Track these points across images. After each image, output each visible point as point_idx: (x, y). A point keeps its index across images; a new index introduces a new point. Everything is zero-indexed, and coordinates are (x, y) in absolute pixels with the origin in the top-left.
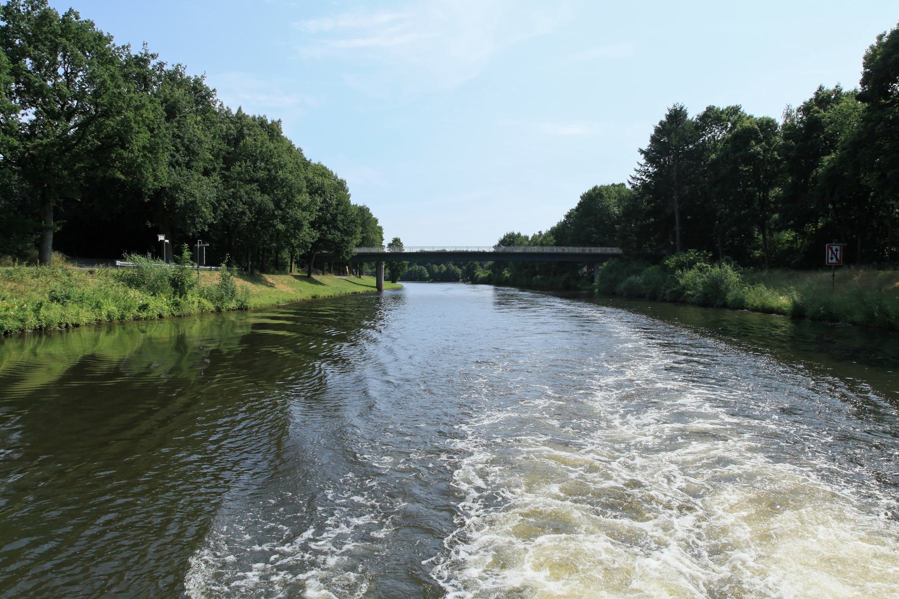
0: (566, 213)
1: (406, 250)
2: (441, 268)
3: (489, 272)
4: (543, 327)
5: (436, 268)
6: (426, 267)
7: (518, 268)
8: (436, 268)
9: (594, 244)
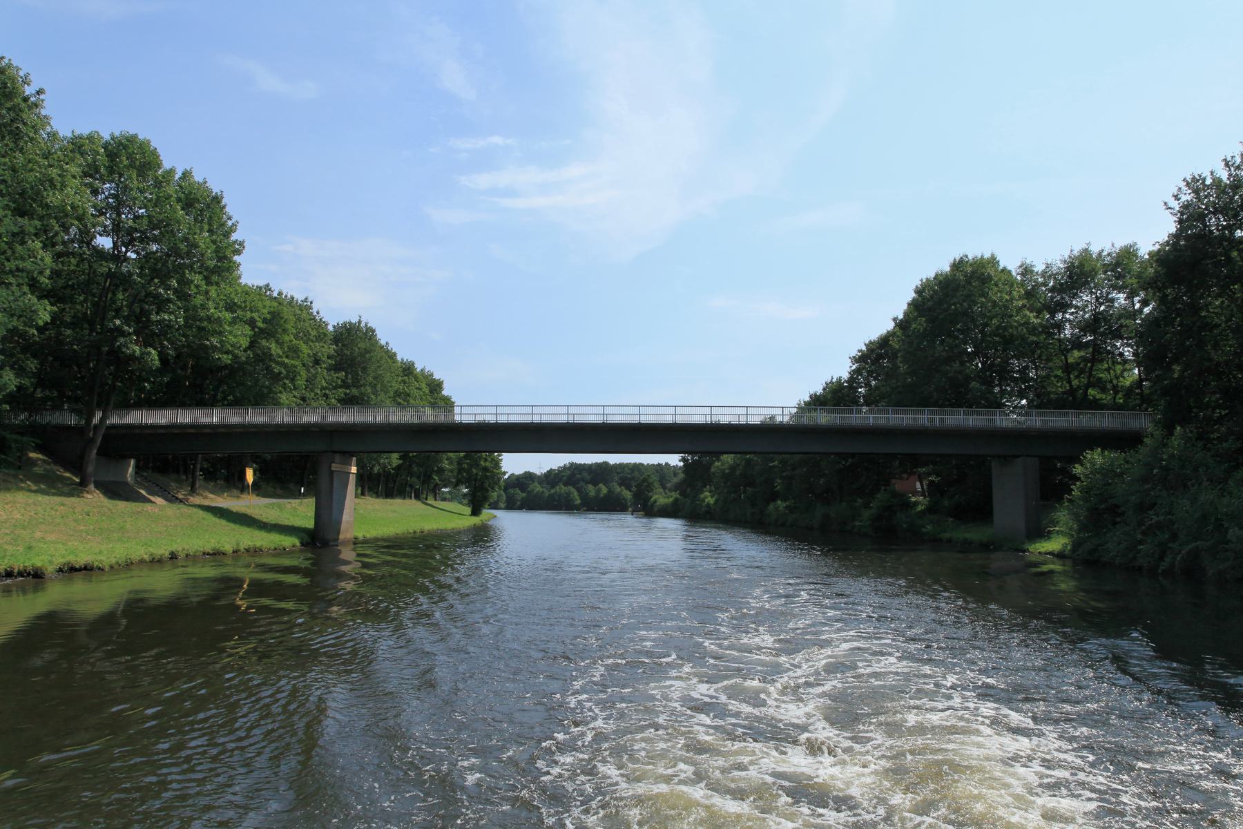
0: (854, 353)
1: (464, 415)
2: (599, 490)
3: (675, 495)
6: (579, 490)
8: (591, 491)
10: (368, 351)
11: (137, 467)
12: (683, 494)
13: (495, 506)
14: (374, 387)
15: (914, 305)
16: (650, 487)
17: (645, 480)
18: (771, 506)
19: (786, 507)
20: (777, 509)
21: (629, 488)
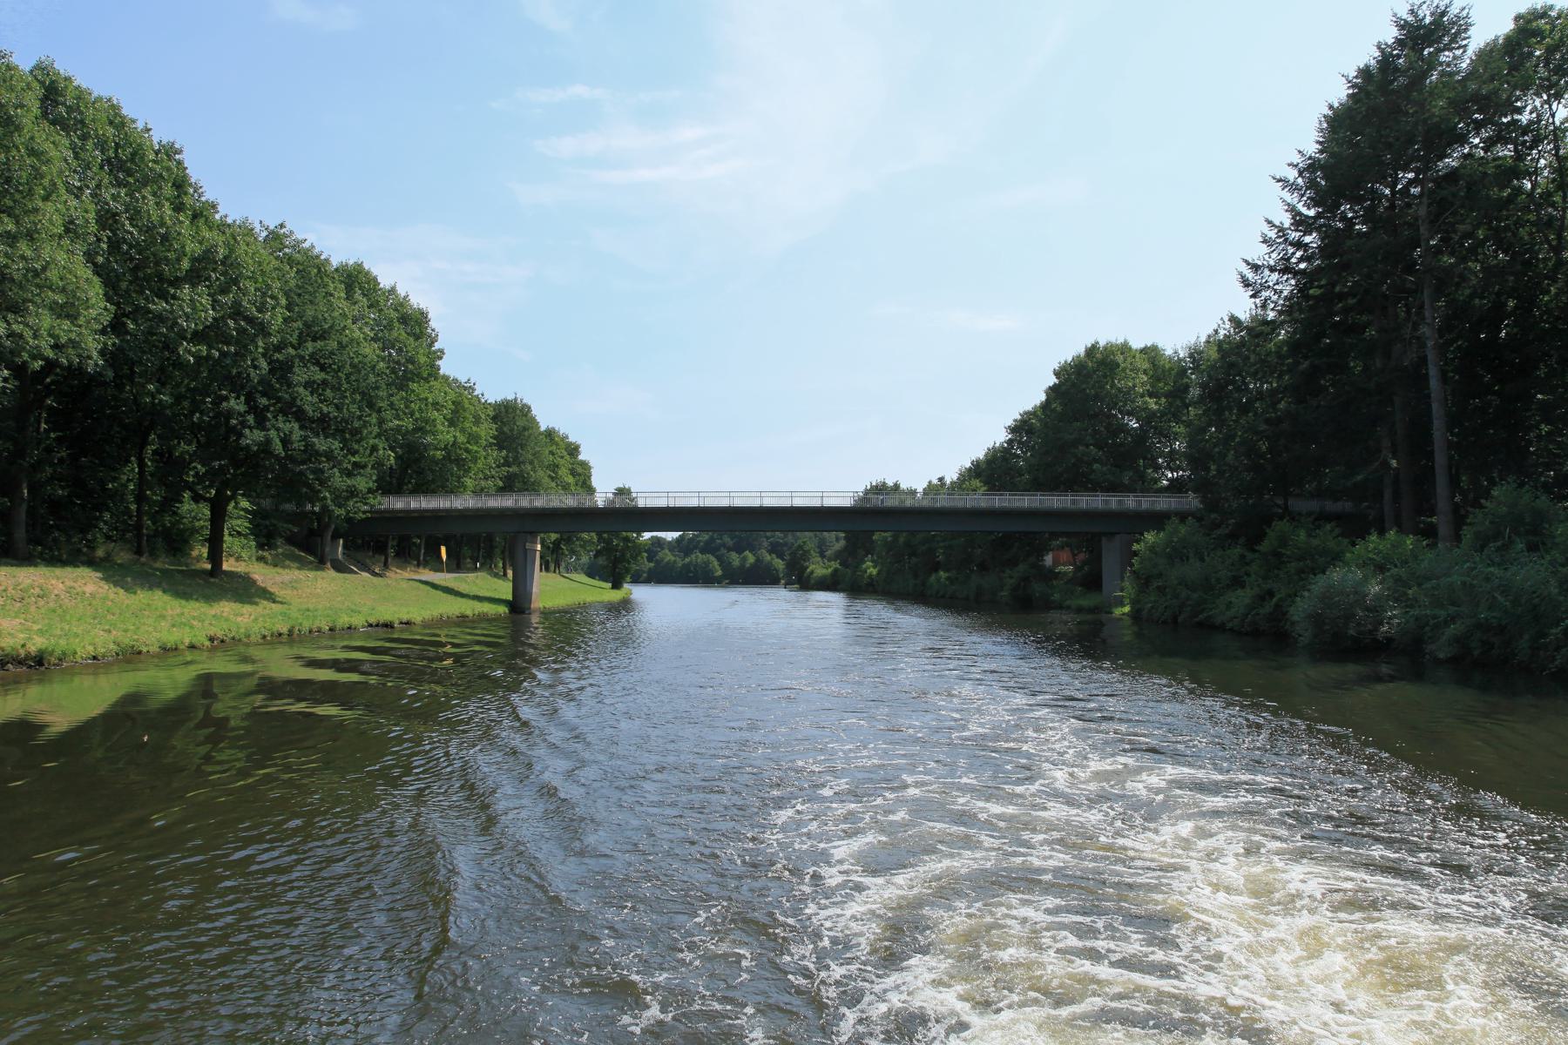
0: (1010, 422)
1: (641, 503)
2: (745, 559)
3: (835, 565)
4: (971, 684)
5: (735, 558)
6: (719, 559)
7: (885, 550)
8: (735, 558)
9: (1095, 487)
10: (525, 429)
11: (345, 547)
12: (844, 564)
13: (636, 580)
14: (531, 463)
15: (1053, 391)
16: (805, 556)
17: (800, 547)
18: (933, 578)
19: (948, 578)
20: (938, 580)
21: (780, 556)
